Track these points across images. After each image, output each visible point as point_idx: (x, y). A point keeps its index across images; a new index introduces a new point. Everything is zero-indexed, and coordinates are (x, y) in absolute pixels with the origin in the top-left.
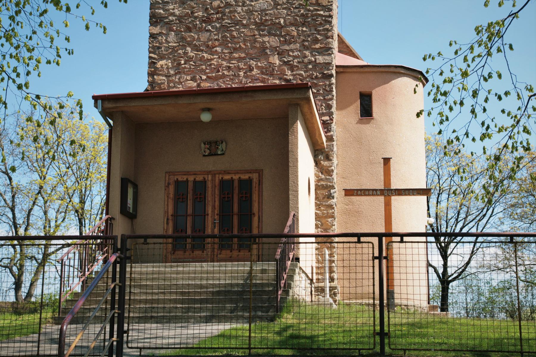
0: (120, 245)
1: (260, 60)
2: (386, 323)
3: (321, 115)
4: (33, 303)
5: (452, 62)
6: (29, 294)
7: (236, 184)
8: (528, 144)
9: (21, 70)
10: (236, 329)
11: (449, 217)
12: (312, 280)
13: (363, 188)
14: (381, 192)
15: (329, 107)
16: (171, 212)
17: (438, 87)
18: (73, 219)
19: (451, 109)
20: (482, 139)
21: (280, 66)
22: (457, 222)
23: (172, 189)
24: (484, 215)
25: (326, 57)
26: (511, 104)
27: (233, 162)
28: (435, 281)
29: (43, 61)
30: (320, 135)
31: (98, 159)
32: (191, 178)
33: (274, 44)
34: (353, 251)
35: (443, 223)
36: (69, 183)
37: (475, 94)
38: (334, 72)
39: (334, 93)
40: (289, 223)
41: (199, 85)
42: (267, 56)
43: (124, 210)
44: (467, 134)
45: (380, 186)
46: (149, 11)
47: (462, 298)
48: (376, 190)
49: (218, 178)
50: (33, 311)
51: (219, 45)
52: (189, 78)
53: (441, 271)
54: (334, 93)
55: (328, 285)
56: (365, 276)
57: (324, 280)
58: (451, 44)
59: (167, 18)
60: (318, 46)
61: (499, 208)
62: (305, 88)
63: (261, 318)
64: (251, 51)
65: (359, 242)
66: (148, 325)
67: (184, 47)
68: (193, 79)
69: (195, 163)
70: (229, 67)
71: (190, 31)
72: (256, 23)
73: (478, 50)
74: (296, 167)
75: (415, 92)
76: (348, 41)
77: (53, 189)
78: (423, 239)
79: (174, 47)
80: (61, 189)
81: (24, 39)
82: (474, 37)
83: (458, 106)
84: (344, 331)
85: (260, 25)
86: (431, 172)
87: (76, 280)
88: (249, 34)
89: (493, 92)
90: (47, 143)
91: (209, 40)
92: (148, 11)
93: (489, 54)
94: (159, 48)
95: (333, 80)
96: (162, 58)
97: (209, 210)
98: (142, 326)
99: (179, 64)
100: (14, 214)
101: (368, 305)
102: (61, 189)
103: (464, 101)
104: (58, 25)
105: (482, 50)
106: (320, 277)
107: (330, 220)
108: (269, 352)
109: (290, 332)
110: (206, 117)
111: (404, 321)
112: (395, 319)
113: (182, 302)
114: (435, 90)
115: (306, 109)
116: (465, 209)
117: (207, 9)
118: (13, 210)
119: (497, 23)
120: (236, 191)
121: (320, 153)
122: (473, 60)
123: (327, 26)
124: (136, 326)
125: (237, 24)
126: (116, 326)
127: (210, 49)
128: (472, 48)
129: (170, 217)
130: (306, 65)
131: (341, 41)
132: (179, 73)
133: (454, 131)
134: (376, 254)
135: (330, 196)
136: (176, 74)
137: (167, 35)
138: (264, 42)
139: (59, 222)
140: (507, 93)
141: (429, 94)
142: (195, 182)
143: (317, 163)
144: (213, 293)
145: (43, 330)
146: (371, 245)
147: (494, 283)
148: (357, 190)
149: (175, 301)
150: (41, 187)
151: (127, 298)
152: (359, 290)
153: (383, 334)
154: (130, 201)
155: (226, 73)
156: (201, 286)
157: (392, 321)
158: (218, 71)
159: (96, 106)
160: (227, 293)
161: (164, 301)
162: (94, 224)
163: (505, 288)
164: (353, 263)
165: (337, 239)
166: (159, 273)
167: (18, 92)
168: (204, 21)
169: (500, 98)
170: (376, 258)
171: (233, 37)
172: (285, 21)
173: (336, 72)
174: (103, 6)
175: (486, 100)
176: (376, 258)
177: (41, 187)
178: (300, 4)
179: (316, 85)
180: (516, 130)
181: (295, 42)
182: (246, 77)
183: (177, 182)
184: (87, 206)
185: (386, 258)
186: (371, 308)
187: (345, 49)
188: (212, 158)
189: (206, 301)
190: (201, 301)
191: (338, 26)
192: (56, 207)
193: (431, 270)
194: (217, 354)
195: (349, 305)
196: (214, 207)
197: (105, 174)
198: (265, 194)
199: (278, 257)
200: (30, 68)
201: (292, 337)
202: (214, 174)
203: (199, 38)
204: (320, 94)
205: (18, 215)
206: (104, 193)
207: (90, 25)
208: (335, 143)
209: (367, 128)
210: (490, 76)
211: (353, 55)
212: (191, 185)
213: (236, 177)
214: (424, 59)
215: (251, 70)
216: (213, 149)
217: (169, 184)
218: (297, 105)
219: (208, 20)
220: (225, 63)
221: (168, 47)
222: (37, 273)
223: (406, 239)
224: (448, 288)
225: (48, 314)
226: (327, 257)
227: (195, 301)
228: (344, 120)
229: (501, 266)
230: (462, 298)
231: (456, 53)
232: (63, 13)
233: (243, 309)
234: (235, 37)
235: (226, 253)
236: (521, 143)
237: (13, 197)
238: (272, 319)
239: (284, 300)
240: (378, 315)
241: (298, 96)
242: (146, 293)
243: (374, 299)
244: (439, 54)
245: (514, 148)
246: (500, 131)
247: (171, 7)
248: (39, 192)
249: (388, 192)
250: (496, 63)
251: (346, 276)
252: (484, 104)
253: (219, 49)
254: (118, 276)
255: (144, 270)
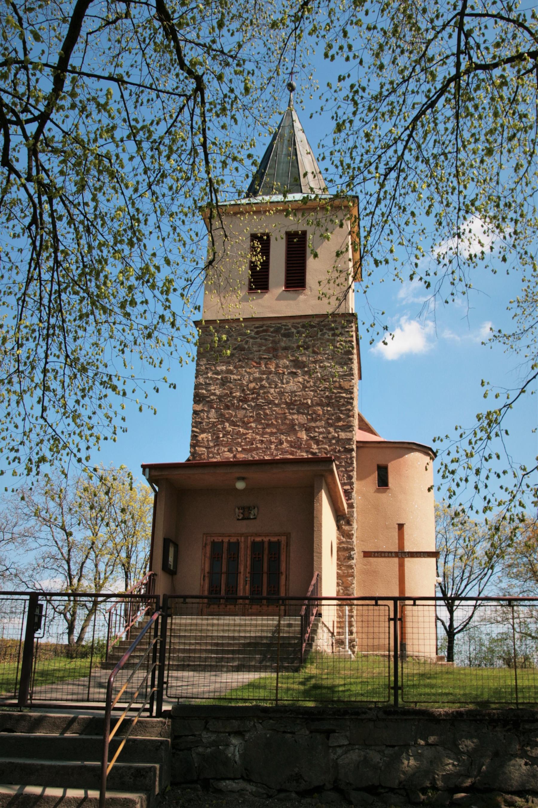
0: (161, 599)
1: (289, 435)
2: (399, 674)
3: (343, 485)
4: (83, 646)
5: (458, 444)
6: (80, 638)
7: (266, 545)
8: (523, 516)
9: (83, 445)
10: (265, 678)
11: (455, 575)
12: (333, 634)
13: (380, 550)
14: (396, 554)
15: (350, 477)
16: (207, 569)
17: (446, 466)
18: (120, 571)
19: (458, 485)
20: (484, 512)
21: (307, 440)
22: (462, 580)
23: (208, 549)
24: (485, 574)
25: (348, 434)
26: (508, 481)
27: (266, 525)
28: (442, 633)
29: (102, 437)
30: (342, 502)
31: (144, 519)
32: (226, 540)
33: (302, 422)
34: (371, 613)
35: (450, 580)
36: (118, 540)
37: (478, 472)
38: (354, 447)
39: (355, 465)
40: (314, 582)
41: (235, 456)
42: (295, 432)
43: (165, 567)
44: (471, 507)
45: (395, 548)
46: (193, 391)
47: (465, 648)
48: (391, 552)
49: (250, 539)
50: (84, 655)
51: (254, 422)
52: (226, 449)
53: (447, 624)
54: (355, 465)
55: (347, 636)
56: (382, 630)
57: (343, 633)
58: (456, 429)
59: (209, 397)
60: (340, 424)
61: (498, 568)
62: (329, 461)
63: (287, 669)
64: (282, 427)
65: (376, 604)
66: (186, 674)
67: (223, 423)
68: (230, 451)
69: (231, 527)
70: (262, 441)
71: (229, 409)
72: (286, 403)
73: (480, 435)
74: (320, 531)
75: (426, 469)
76: (367, 419)
77: (104, 544)
78: (432, 602)
79: (214, 422)
80: (110, 545)
81: (86, 420)
82: (476, 424)
83: (464, 482)
84: (362, 682)
85: (290, 405)
86: (440, 536)
87: (122, 629)
88: (280, 412)
89: (493, 471)
90: (99, 502)
91: (245, 416)
92: (192, 392)
93: (489, 438)
94: (201, 423)
95: (354, 454)
96: (203, 431)
97: (242, 569)
98: (180, 674)
99: (218, 437)
100: (69, 566)
101: (384, 656)
102: (110, 545)
103: (469, 478)
104: (116, 407)
105: (484, 435)
106: (341, 630)
107: (350, 579)
108: (293, 704)
109: (313, 681)
110: (240, 485)
111: (415, 672)
112: (408, 669)
113: (217, 652)
114: (443, 468)
115: (330, 480)
116: (469, 569)
117: (244, 390)
118: (68, 562)
119: (496, 412)
120: (266, 552)
121: (342, 518)
122: (476, 443)
123: (349, 407)
124: (175, 674)
125: (269, 404)
126: (157, 672)
127: (245, 425)
128: (475, 434)
129: (206, 575)
130: (330, 440)
131: (361, 419)
132: (218, 445)
133: (460, 505)
134: (392, 616)
135: (350, 558)
136: (215, 446)
137: (208, 412)
138: (293, 419)
139: (108, 574)
140: (505, 472)
141: (439, 471)
142: (229, 543)
143: (339, 527)
144: (244, 645)
145: (92, 674)
146: (387, 608)
147: (494, 636)
148: (375, 552)
149: (211, 651)
150: (93, 543)
151: (167, 647)
152: (376, 642)
153: (396, 688)
154: (171, 559)
155: (259, 445)
156: (234, 638)
157: (405, 671)
158: (252, 444)
159: (144, 473)
160: (256, 645)
161: (201, 651)
162: (138, 579)
163: (503, 637)
164: (371, 618)
165: (355, 602)
166: (196, 625)
167: (78, 465)
168: (241, 401)
169: (499, 476)
170: (391, 619)
171: (266, 414)
172: (312, 402)
173: (357, 447)
174: (155, 391)
175: (487, 477)
176: (391, 619)
177: (93, 543)
178: (325, 388)
179: (338, 458)
180: (512, 504)
181: (321, 420)
182: (277, 449)
183: (213, 543)
184: (133, 561)
185: (400, 619)
186: (387, 659)
187: (365, 427)
188: (245, 522)
189: (238, 652)
190: (233, 652)
191: (358, 407)
192: (106, 561)
193: (439, 623)
194: (247, 704)
195: (366, 656)
196: (246, 566)
197: (149, 532)
198: (292, 555)
199: (303, 613)
200: (90, 444)
201: (316, 687)
202: (246, 536)
203: (236, 416)
204: (342, 466)
205: (73, 567)
206: (148, 549)
207: (143, 408)
208: (355, 510)
209: (383, 497)
210: (490, 457)
211: (370, 431)
212: (225, 546)
213: (266, 539)
214: (434, 441)
215: (281, 443)
216: (246, 514)
217: (206, 544)
218: (322, 476)
219: (245, 400)
220: (258, 437)
221: (209, 423)
222: (87, 620)
223: (418, 602)
224: (453, 640)
225: (97, 659)
226: (347, 613)
227: (228, 652)
228: (363, 489)
229: (499, 619)
230: (465, 648)
231: (461, 436)
232: (120, 397)
233: (272, 660)
234: (267, 415)
235: (255, 608)
236: (517, 515)
237: (69, 551)
238: (297, 670)
239: (307, 652)
240: (392, 666)
241: (323, 468)
242: (185, 644)
243: (389, 651)
244: (447, 437)
245: (512, 520)
246: (499, 504)
247: (213, 388)
248: (92, 547)
249: (402, 555)
250: (494, 446)
251: (365, 630)
252: (486, 481)
253: (253, 425)
254: (160, 627)
255: (183, 621)
